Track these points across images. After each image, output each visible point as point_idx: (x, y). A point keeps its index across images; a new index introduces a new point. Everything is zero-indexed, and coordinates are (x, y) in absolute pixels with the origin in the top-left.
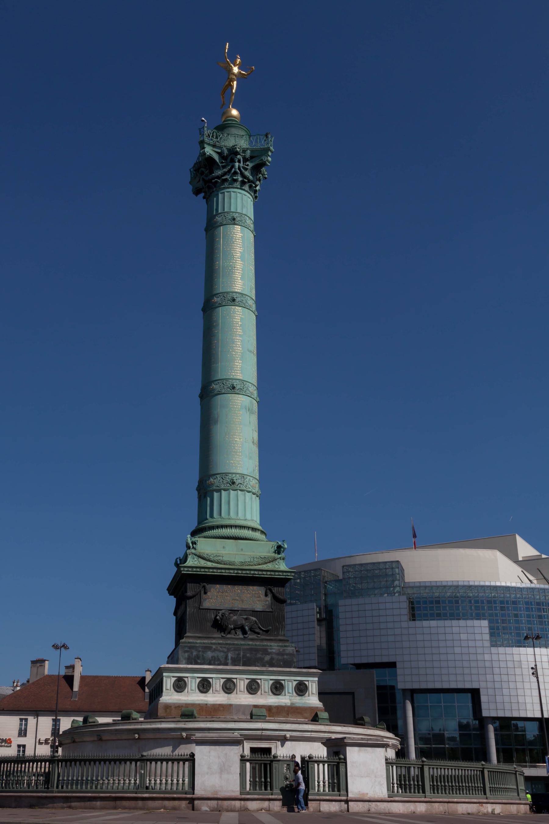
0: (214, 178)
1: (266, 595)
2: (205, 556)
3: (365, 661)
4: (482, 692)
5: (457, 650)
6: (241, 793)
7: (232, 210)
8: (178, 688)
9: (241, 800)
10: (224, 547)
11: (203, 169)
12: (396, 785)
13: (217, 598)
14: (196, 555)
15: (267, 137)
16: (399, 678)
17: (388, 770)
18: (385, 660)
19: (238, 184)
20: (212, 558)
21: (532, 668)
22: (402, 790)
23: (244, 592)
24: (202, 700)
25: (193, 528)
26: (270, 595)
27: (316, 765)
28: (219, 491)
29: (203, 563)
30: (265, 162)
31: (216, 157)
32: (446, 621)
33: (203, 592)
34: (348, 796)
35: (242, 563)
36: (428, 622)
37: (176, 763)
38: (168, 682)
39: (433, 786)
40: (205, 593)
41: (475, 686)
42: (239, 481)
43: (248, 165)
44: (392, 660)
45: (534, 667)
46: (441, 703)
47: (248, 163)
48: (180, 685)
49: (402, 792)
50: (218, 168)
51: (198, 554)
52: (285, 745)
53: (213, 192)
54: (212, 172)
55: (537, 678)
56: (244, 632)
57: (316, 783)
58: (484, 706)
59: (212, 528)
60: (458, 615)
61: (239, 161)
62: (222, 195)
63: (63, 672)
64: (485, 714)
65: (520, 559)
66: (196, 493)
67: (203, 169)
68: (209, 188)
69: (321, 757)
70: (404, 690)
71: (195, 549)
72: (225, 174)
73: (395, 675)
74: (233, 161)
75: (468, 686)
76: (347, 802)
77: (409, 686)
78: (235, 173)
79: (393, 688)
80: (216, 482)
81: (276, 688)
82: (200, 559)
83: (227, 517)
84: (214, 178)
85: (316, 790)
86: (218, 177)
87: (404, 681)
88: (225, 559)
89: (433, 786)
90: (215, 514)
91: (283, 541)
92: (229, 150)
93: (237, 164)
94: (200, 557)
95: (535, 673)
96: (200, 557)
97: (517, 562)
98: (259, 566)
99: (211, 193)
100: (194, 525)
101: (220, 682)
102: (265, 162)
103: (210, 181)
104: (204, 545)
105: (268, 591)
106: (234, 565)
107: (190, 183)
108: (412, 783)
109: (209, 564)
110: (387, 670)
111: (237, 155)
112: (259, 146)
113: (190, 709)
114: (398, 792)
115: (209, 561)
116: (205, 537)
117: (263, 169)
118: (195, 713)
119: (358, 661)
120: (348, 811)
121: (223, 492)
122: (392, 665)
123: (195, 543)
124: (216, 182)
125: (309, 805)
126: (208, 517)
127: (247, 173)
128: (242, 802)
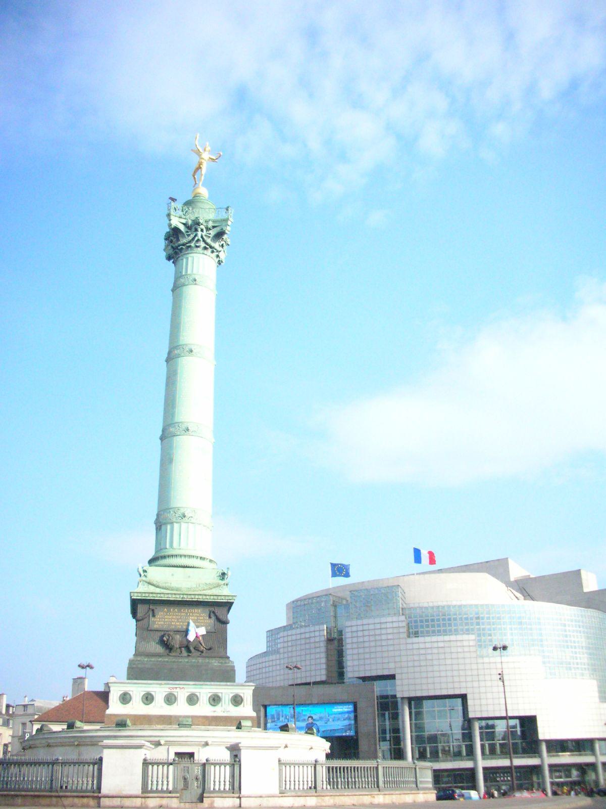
0: (179, 246)
1: (210, 617)
2: (155, 583)
3: (368, 674)
4: (469, 697)
5: (448, 662)
6: (142, 793)
7: (194, 272)
8: (168, 700)
9: (142, 797)
10: (173, 575)
11: (172, 238)
12: (325, 783)
13: (164, 620)
14: (146, 582)
15: (227, 210)
16: (398, 688)
17: (280, 770)
18: (386, 673)
19: (200, 250)
20: (160, 585)
21: (500, 674)
22: (330, 786)
23: (189, 615)
24: (306, 707)
25: (150, 557)
26: (213, 618)
27: (284, 767)
28: (172, 523)
29: (152, 589)
30: (225, 231)
31: (182, 228)
32: (451, 636)
33: (151, 615)
34: (240, 793)
35: (189, 589)
36: (429, 638)
37: (223, 767)
38: (114, 698)
39: (385, 781)
40: (154, 616)
41: (463, 692)
42: (190, 515)
43: (210, 234)
44: (391, 673)
45: (501, 673)
46: (437, 707)
47: (210, 232)
48: (125, 698)
49: (330, 788)
50: (184, 236)
51: (148, 581)
52: (226, 750)
53: (179, 257)
54: (178, 240)
55: (503, 682)
56: (189, 650)
57: (284, 783)
58: (470, 709)
59: (164, 557)
60: (450, 631)
61: (202, 230)
62: (192, 258)
63: (101, 689)
64: (471, 715)
65: (512, 579)
66: (154, 526)
67: (172, 238)
68: (176, 253)
69: (155, 759)
70: (402, 698)
71: (145, 576)
72: (190, 242)
73: (395, 685)
74: (196, 230)
75: (457, 692)
76: (240, 798)
77: (406, 695)
78: (198, 240)
79: (394, 696)
80: (171, 515)
81: (214, 700)
82: (150, 586)
83: (178, 547)
84: (179, 246)
85: (284, 789)
86: (184, 245)
87: (403, 689)
88: (174, 585)
89: (385, 781)
90: (175, 544)
91: (228, 568)
92: (193, 221)
93: (199, 233)
94: (149, 583)
95: (502, 679)
96: (149, 583)
97: (509, 584)
98: (204, 592)
99: (178, 258)
100: (151, 554)
101: (140, 694)
102: (225, 231)
103: (177, 248)
104: (157, 574)
105: (212, 614)
106: (180, 590)
107: (164, 250)
108: (363, 780)
109: (158, 590)
110: (389, 682)
111: (199, 226)
112: (220, 218)
113: (125, 718)
114: (326, 788)
115: (158, 587)
116: (156, 566)
117: (225, 237)
118: (129, 722)
119: (362, 675)
120: (240, 806)
121: (175, 524)
122: (393, 677)
123: (146, 572)
124: (182, 248)
125: (204, 801)
126: (168, 546)
127: (209, 241)
128: (143, 800)
